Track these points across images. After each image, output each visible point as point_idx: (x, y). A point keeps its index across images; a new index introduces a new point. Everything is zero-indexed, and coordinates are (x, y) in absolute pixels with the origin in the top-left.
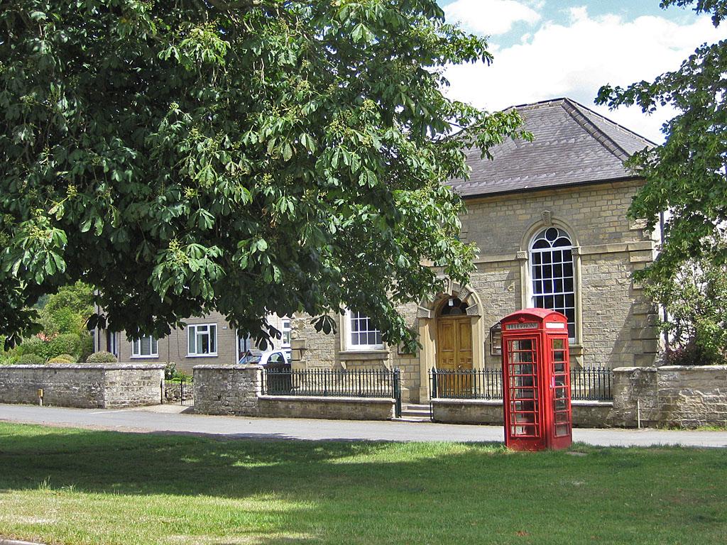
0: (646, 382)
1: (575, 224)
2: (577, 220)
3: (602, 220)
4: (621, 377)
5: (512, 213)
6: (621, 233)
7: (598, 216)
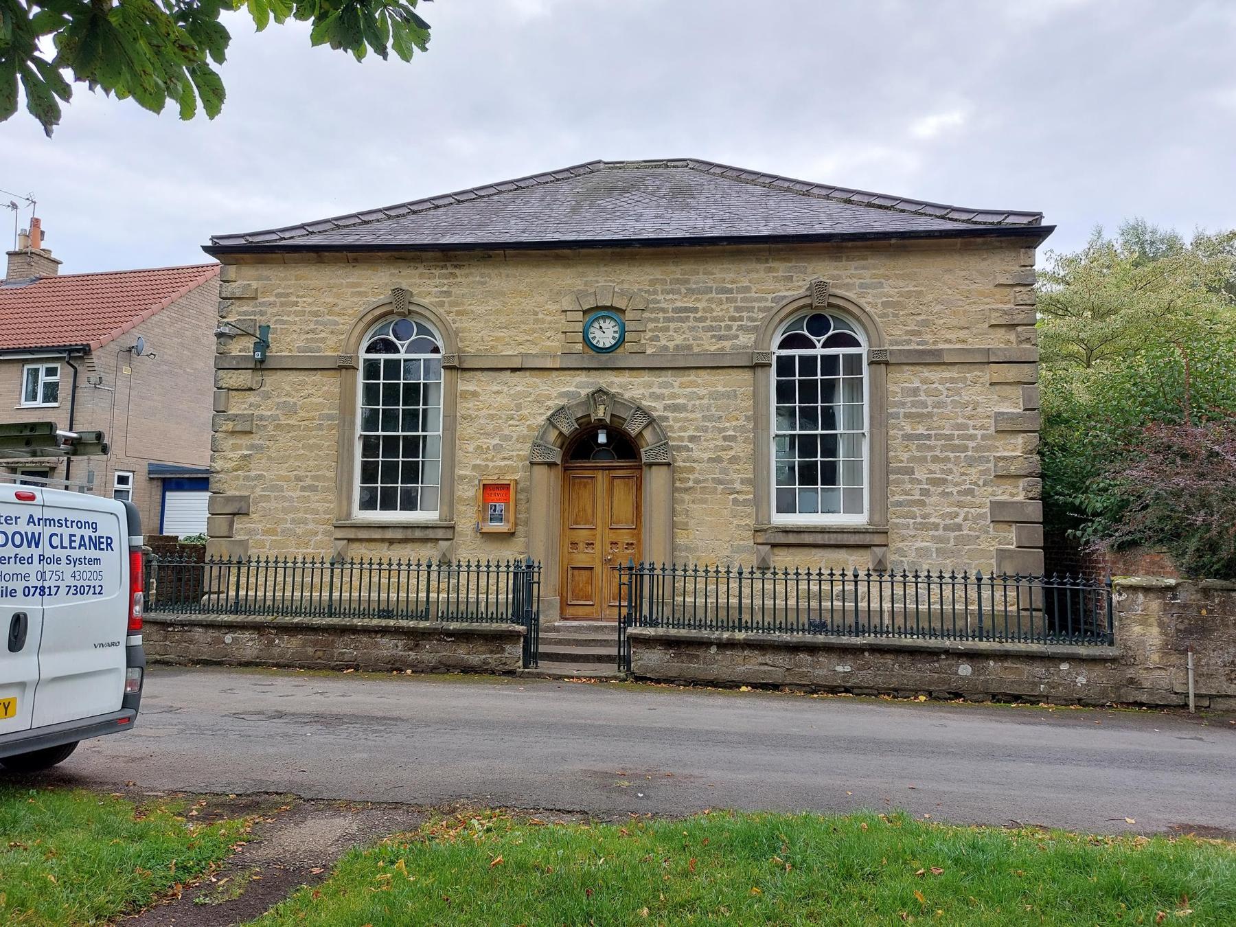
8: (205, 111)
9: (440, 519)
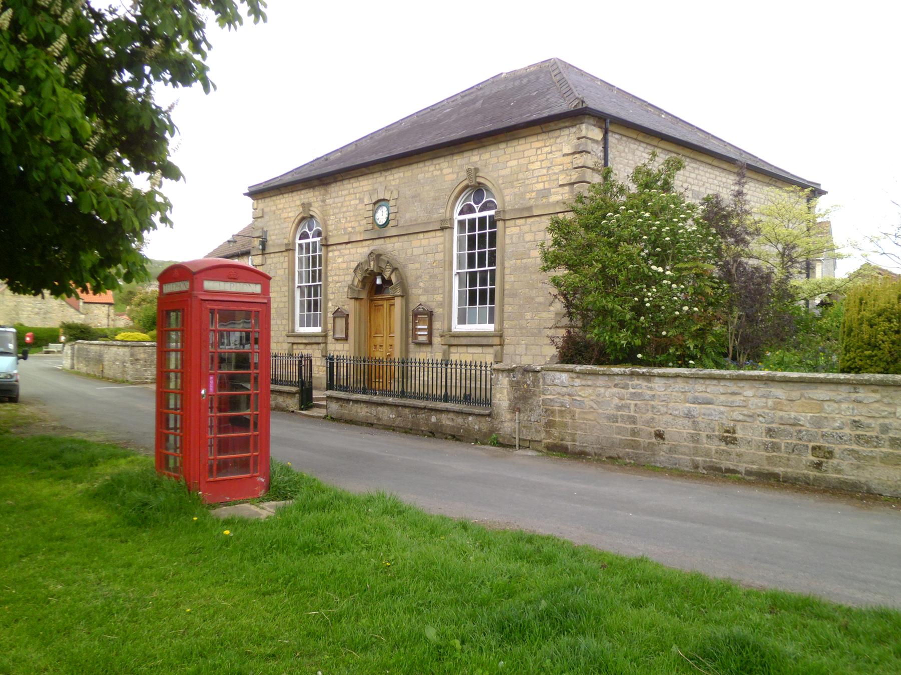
0: (528, 385)
1: (501, 182)
2: (503, 176)
3: (529, 174)
4: (501, 376)
5: (438, 173)
6: (549, 189)
7: (525, 170)
8: (169, 179)
9: (495, 331)
